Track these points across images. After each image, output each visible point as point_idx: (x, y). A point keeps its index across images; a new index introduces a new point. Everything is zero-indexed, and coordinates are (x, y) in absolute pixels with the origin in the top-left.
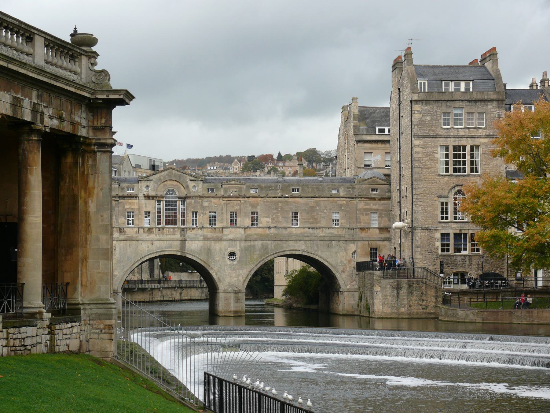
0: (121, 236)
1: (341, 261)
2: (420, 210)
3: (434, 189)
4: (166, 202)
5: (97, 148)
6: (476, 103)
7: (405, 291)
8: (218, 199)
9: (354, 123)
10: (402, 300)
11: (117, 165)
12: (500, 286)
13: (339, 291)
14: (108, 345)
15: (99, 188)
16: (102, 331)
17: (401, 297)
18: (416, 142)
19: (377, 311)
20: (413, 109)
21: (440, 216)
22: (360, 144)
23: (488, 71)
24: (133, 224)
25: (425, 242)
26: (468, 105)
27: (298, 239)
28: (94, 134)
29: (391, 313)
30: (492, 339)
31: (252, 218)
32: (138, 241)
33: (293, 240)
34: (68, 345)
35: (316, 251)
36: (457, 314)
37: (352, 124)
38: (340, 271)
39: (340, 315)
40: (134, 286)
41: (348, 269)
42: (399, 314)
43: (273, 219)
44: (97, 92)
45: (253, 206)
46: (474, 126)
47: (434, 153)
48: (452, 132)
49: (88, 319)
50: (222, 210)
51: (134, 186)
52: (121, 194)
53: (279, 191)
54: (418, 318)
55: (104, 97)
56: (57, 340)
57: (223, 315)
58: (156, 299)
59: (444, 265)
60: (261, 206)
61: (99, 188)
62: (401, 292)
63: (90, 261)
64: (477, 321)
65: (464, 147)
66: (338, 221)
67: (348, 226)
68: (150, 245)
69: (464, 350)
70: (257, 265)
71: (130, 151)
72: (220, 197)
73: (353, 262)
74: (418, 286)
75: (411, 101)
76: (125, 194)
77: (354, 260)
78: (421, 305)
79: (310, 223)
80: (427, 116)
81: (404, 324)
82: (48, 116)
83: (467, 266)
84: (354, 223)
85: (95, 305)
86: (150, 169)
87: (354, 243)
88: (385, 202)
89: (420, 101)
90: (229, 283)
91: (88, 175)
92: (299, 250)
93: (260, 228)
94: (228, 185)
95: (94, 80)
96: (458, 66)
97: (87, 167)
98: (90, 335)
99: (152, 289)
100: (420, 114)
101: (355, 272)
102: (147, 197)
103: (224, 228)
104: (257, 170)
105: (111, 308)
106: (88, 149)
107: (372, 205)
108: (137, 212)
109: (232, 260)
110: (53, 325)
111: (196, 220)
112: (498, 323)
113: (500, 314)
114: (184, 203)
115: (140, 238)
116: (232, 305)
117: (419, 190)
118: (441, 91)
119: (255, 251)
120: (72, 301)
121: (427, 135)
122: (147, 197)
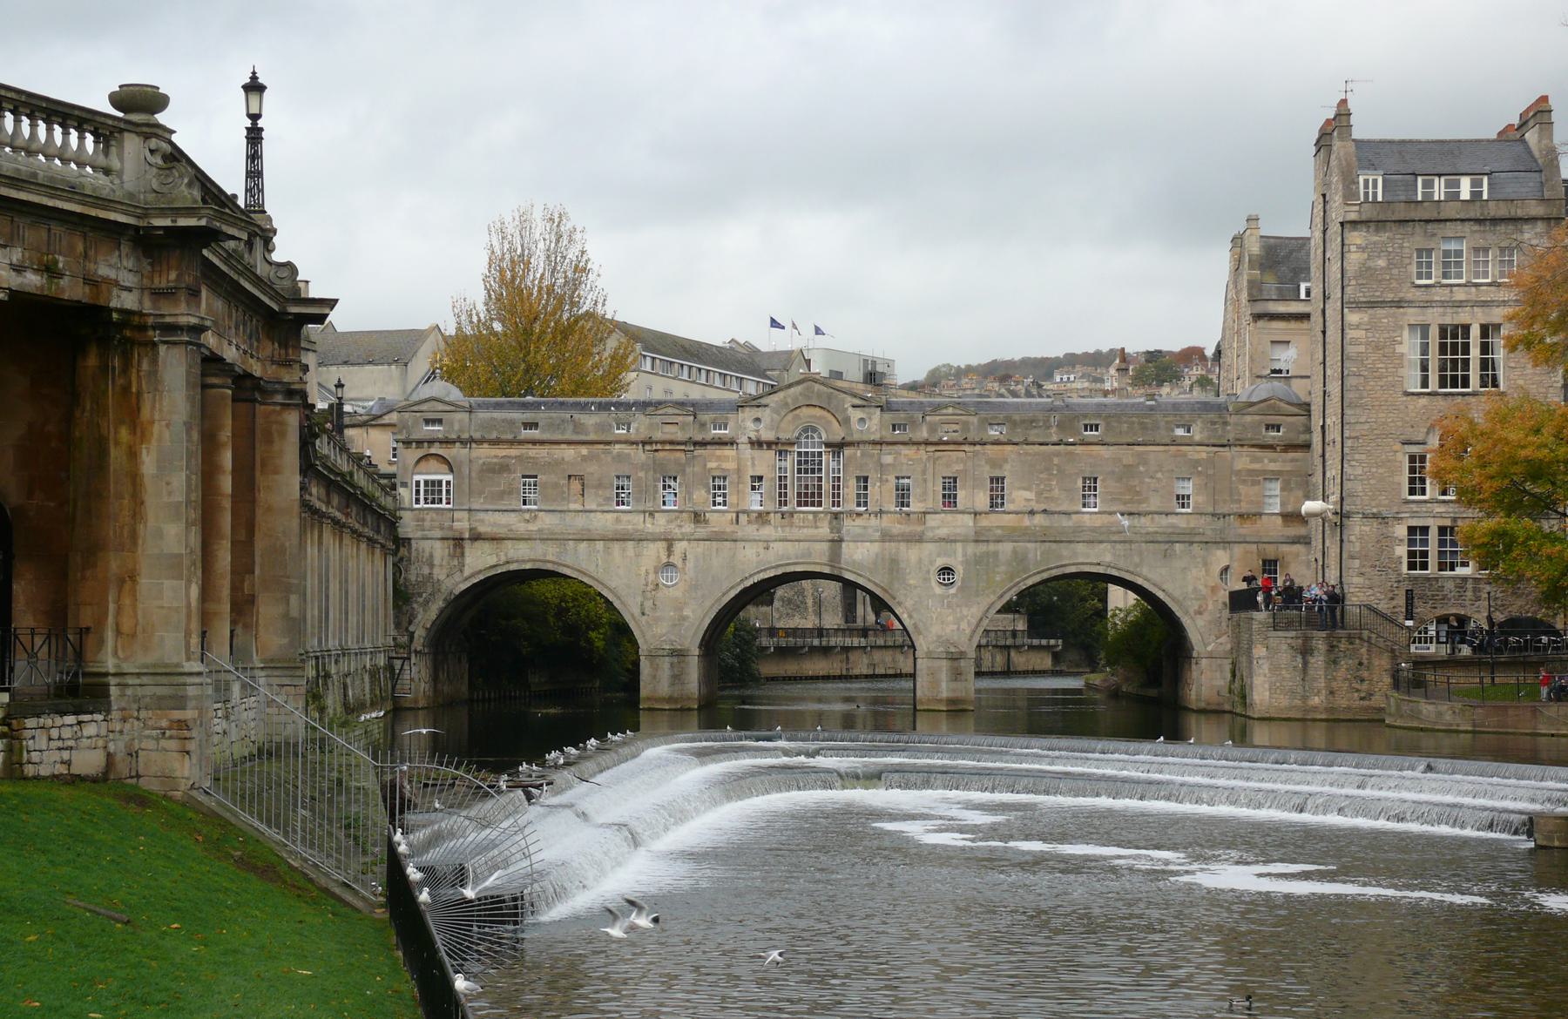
0: (698, 530)
1: (1195, 590)
2: (1360, 472)
3: (1392, 424)
4: (799, 454)
5: (160, 335)
6: (1495, 225)
7: (1322, 658)
8: (915, 447)
9: (1249, 275)
10: (1315, 680)
11: (776, 373)
12: (1545, 648)
13: (1191, 657)
14: (177, 765)
15: (164, 423)
16: (164, 733)
17: (1311, 672)
18: (1353, 318)
19: (1258, 702)
20: (1346, 242)
21: (1406, 486)
22: (1261, 323)
23: (1530, 152)
24: (725, 505)
25: (1370, 545)
26: (1476, 231)
27: (1096, 537)
28: (155, 305)
29: (1291, 708)
30: (1429, 768)
31: (992, 490)
32: (736, 541)
33: (1084, 542)
34: (68, 763)
35: (1137, 566)
36: (1420, 712)
37: (1245, 277)
38: (1191, 611)
39: (1193, 711)
40: (800, 641)
41: (1210, 607)
42: (1306, 711)
43: (1039, 494)
44: (150, 212)
45: (994, 463)
46: (1489, 280)
47: (1394, 342)
48: (1439, 295)
49: (135, 706)
50: (924, 472)
51: (727, 418)
52: (699, 438)
53: (1054, 430)
54: (1350, 720)
55: (167, 222)
56: (29, 752)
57: (926, 707)
58: (856, 672)
59: (1415, 600)
60: (1012, 462)
61: (164, 423)
62: (1312, 660)
63: (143, 581)
64: (1461, 728)
65: (1466, 328)
66: (1188, 496)
67: (1210, 510)
68: (762, 551)
69: (1361, 792)
70: (1002, 596)
71: (821, 341)
72: (918, 444)
73: (1222, 592)
74: (1351, 647)
75: (1342, 224)
76: (708, 438)
77: (1226, 587)
78: (1358, 691)
79: (1125, 503)
80: (1379, 257)
81: (1318, 735)
82: (8, 267)
83: (1467, 603)
84: (1225, 502)
85: (151, 677)
86: (865, 382)
87: (1224, 548)
88: (1298, 455)
89: (1361, 222)
90: (939, 637)
91: (139, 394)
92: (1099, 564)
93: (1009, 513)
94: (938, 418)
95: (155, 187)
96: (1460, 141)
97: (139, 377)
98: (140, 742)
99: (846, 649)
100: (1363, 252)
101: (1226, 613)
102: (757, 444)
103: (929, 513)
104: (1164, 381)
105: (185, 685)
106: (138, 336)
107: (1266, 461)
108: (735, 476)
109: (945, 585)
110: (16, 718)
111: (866, 496)
112: (1507, 733)
113: (1511, 712)
114: (839, 457)
115: (740, 535)
116: (944, 685)
117: (1358, 427)
118: (1414, 198)
119: (997, 566)
120: (93, 667)
121: (1378, 302)
122: (757, 444)
